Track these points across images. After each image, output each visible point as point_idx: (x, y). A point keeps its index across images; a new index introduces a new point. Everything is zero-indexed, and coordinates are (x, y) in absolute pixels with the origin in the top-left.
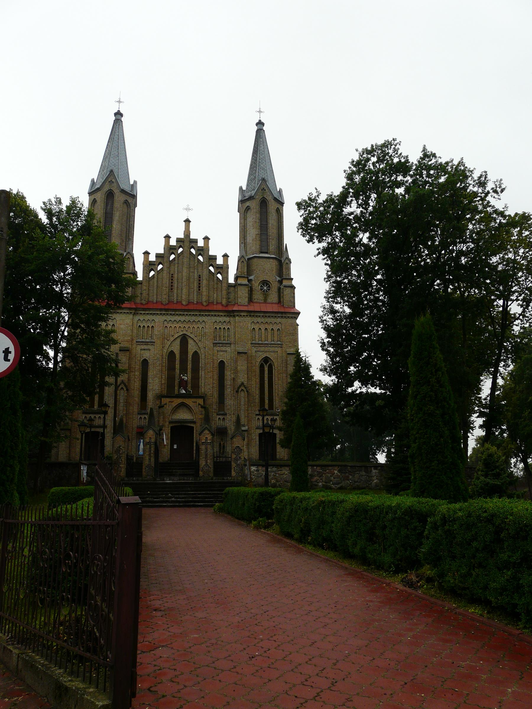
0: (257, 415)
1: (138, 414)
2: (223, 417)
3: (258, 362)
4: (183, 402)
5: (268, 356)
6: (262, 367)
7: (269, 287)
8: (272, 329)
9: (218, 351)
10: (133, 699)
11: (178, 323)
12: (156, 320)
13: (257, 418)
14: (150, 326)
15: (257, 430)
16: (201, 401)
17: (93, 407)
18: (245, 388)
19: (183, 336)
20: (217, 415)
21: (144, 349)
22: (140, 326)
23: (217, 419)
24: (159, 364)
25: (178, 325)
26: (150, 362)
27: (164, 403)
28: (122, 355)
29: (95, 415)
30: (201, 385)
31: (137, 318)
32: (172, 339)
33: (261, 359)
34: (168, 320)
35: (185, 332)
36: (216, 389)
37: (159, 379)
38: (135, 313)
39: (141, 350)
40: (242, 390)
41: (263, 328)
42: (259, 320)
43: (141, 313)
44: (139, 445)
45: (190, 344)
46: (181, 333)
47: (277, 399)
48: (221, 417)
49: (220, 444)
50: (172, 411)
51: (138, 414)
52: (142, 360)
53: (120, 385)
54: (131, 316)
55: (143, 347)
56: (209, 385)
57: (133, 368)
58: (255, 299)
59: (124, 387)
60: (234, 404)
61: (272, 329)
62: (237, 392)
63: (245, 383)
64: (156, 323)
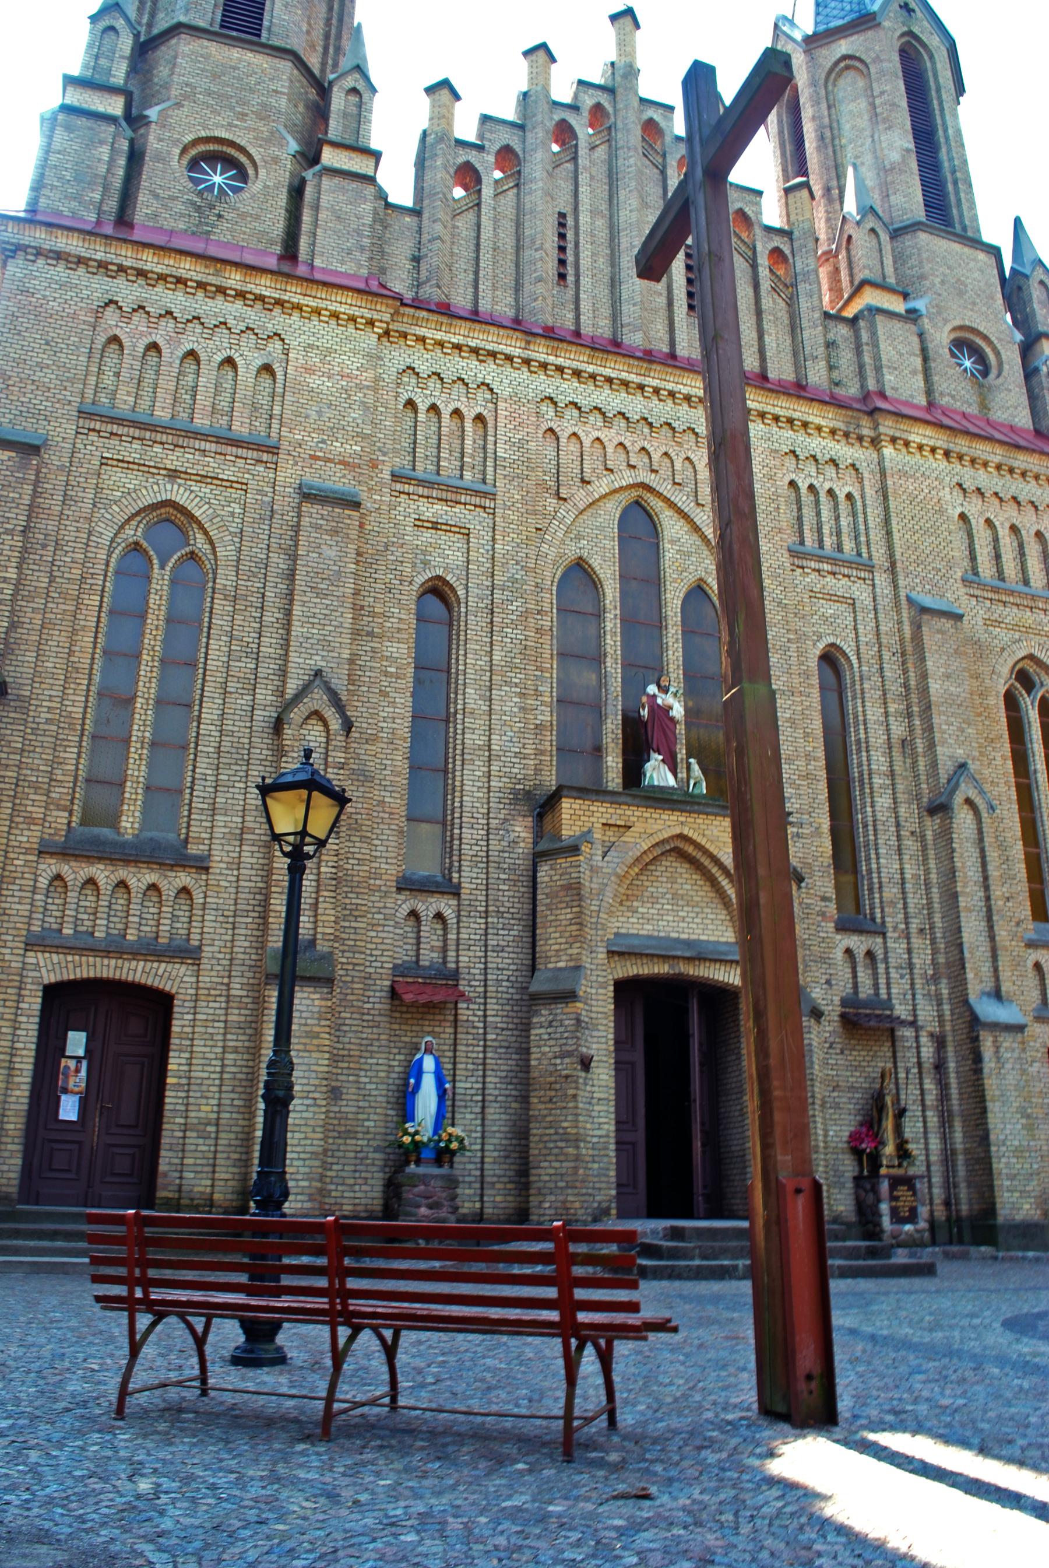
0: (1031, 945)
2: (114, 878)
4: (681, 837)
5: (1037, 653)
6: (1011, 701)
7: (243, 176)
8: (229, 361)
9: (813, 594)
11: (126, 316)
12: (503, 390)
14: (469, 414)
19: (634, 493)
21: (435, 526)
22: (410, 404)
24: (525, 615)
25: (611, 436)
27: (576, 831)
29: (122, 873)
31: (397, 357)
32: (581, 497)
34: (562, 400)
35: (644, 476)
37: (522, 695)
38: (387, 333)
39: (420, 524)
41: (249, 360)
42: (983, 478)
43: (422, 340)
45: (672, 542)
46: (627, 478)
48: (858, 943)
52: (420, 580)
53: (298, 697)
54: (369, 339)
55: (432, 510)
57: (373, 614)
58: (942, 394)
59: (330, 713)
61: (229, 361)
64: (501, 405)
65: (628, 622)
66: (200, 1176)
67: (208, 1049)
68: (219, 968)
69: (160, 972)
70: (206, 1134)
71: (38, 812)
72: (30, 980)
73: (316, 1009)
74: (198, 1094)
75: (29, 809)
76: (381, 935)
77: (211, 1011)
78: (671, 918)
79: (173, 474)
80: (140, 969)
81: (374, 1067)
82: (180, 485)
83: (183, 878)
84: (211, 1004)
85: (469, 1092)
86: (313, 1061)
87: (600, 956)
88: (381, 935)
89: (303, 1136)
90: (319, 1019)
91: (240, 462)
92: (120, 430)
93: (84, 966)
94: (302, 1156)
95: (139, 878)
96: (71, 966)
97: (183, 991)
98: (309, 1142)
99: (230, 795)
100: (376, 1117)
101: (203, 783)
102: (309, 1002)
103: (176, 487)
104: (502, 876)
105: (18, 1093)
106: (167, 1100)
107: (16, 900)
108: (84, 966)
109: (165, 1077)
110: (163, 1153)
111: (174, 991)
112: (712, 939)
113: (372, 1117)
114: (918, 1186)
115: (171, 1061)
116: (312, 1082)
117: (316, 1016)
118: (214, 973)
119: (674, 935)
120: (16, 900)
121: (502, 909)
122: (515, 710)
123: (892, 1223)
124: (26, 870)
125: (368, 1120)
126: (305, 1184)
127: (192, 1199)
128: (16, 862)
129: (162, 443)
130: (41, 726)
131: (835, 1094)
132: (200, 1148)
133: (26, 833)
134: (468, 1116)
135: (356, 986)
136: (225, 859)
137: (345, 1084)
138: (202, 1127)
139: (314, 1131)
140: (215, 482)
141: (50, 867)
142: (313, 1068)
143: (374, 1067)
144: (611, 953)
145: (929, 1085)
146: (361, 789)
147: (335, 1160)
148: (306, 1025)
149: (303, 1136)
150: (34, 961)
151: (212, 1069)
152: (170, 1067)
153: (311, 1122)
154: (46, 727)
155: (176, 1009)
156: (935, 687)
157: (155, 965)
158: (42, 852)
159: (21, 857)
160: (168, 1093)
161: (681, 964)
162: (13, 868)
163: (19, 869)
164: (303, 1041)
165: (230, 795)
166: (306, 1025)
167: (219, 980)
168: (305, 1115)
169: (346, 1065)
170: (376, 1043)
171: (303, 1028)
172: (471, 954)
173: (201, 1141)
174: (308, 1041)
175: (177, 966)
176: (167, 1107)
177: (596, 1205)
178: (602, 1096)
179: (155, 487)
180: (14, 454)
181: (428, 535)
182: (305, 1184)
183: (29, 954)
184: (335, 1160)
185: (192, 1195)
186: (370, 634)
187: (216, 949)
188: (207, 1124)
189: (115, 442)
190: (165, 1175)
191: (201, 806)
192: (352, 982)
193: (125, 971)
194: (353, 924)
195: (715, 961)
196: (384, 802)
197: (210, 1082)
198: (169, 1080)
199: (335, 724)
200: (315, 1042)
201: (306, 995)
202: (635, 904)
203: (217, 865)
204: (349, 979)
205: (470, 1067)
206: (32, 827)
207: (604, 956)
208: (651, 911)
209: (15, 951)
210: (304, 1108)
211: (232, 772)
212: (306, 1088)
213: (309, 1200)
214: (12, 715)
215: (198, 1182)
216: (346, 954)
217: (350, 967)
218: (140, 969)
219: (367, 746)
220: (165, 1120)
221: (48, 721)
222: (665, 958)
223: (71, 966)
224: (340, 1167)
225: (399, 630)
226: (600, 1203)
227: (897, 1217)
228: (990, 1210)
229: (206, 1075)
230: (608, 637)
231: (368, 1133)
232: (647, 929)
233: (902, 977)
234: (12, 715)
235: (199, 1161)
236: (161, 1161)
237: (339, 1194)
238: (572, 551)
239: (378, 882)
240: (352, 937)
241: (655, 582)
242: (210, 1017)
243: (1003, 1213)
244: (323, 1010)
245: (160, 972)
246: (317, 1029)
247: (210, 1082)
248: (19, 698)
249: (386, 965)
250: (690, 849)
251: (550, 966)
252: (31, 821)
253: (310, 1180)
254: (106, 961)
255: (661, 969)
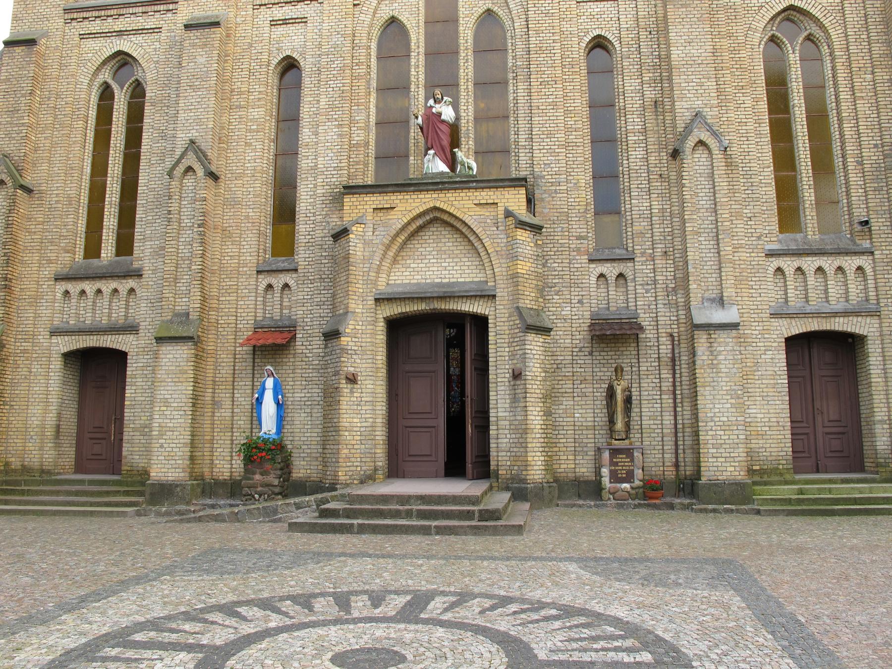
0: (771, 254)
1: (259, 272)
2: (616, 272)
3: (756, 31)
4: (436, 209)
10: (443, 117)
13: (771, 270)
15: (775, 323)
16: (515, 200)
17: (98, 256)
18: (715, 134)
20: (591, 261)
21: (285, 22)
23: (593, 279)
26: (307, 65)
28: (194, 45)
30: (517, 142)
33: (768, 16)
36: (583, 152)
37: (340, 126)
39: (274, 23)
40: (701, 143)
44: (259, 401)
47: (854, 178)
48: (611, 270)
49: (611, 393)
50: (388, 247)
51: (259, 272)
52: (275, 61)
56: (550, 135)
57: (240, 93)
59: (197, 166)
60: (663, 210)
62: (675, 154)
63: (710, 114)
65: (430, 55)
66: (142, 457)
67: (144, 383)
68: (149, 334)
69: (120, 341)
70: (144, 433)
71: (53, 256)
72: (54, 352)
73: (185, 356)
74: (140, 410)
75: (49, 255)
76: (246, 303)
77: (145, 361)
78: (436, 269)
79: (120, 33)
80: (109, 339)
81: (243, 387)
82: (124, 40)
83: (131, 283)
84: (145, 357)
85: (303, 399)
86: (184, 388)
87: (369, 303)
88: (246, 303)
89: (178, 433)
90: (187, 362)
91: (157, 15)
92: (75, 16)
93: (81, 341)
94: (178, 445)
95: (107, 286)
96: (74, 341)
97: (132, 350)
98: (182, 437)
99: (154, 228)
100: (245, 418)
101: (140, 223)
102: (181, 352)
103: (122, 41)
104: (324, 254)
105: (51, 415)
106: (125, 414)
107: (44, 308)
108: (81, 341)
109: (124, 401)
110: (124, 445)
111: (127, 351)
112: (468, 280)
113: (242, 418)
114: (636, 454)
115: (127, 391)
116: (183, 400)
117: (185, 360)
118: (147, 338)
119: (437, 281)
120: (44, 308)
121: (323, 276)
122: (335, 137)
123: (611, 482)
124: (49, 290)
125: (240, 420)
126: (180, 462)
127: (138, 471)
128: (44, 286)
129: (112, 16)
130: (53, 206)
131: (583, 386)
132: (142, 441)
133: (48, 269)
134: (302, 415)
135: (229, 337)
136: (151, 268)
137: (223, 399)
138: (142, 429)
139: (185, 431)
140: (144, 32)
141: (61, 287)
142: (184, 392)
143: (243, 387)
144: (377, 300)
145: (666, 374)
146: (232, 210)
147: (219, 446)
148: (179, 366)
149: (178, 433)
150: (56, 341)
151: (147, 395)
152: (126, 395)
153: (183, 425)
154: (56, 206)
155: (128, 361)
156: (676, 54)
157: (117, 336)
158: (58, 279)
159: (46, 283)
160: (125, 410)
161: (435, 302)
162: (42, 290)
163: (45, 290)
164: (178, 376)
165: (154, 228)
166: (179, 366)
167: (150, 342)
168: (179, 421)
169: (224, 387)
170: (244, 372)
171: (178, 368)
172: (305, 308)
173: (142, 437)
174: (180, 376)
175: (128, 336)
176: (126, 418)
177: (362, 473)
178: (368, 399)
179: (111, 45)
180: (24, 47)
181: (281, 30)
182: (180, 462)
183: (53, 337)
184: (219, 446)
185: (138, 469)
186: (240, 107)
187: (148, 323)
188: (145, 428)
189: (86, 23)
190: (126, 457)
191: (139, 237)
192: (227, 335)
193: (101, 341)
194: (227, 298)
195: (463, 297)
196: (248, 216)
197: (146, 403)
198: (126, 403)
199: (200, 172)
200: (185, 376)
201: (179, 348)
202: (408, 262)
203: (147, 273)
204: (226, 333)
205: (304, 383)
206: (51, 265)
207: (373, 302)
208: (420, 265)
209: (45, 337)
210: (179, 417)
211: (154, 214)
212: (180, 404)
213: (183, 472)
214: (37, 202)
215: (140, 461)
216: (223, 318)
217: (226, 326)
218: (109, 339)
219: (236, 182)
220: (125, 426)
221: (57, 202)
222: (422, 299)
223: (74, 341)
224: (222, 450)
225: (259, 99)
226: (365, 471)
227: (615, 477)
228: (698, 474)
229: (143, 399)
230: (413, 70)
231: (240, 428)
232: (417, 279)
233: (647, 291)
234: (37, 202)
235: (141, 449)
236: (123, 449)
237: (222, 466)
238: (385, 13)
239: (245, 269)
240: (227, 306)
241: (452, 20)
242: (145, 365)
243: (706, 475)
244: (189, 356)
245: (120, 341)
246: (186, 368)
247: (146, 403)
248: (40, 192)
249: (249, 322)
250: (445, 217)
251: (337, 313)
252: (50, 262)
253: (183, 460)
254: (92, 337)
255: (422, 307)
